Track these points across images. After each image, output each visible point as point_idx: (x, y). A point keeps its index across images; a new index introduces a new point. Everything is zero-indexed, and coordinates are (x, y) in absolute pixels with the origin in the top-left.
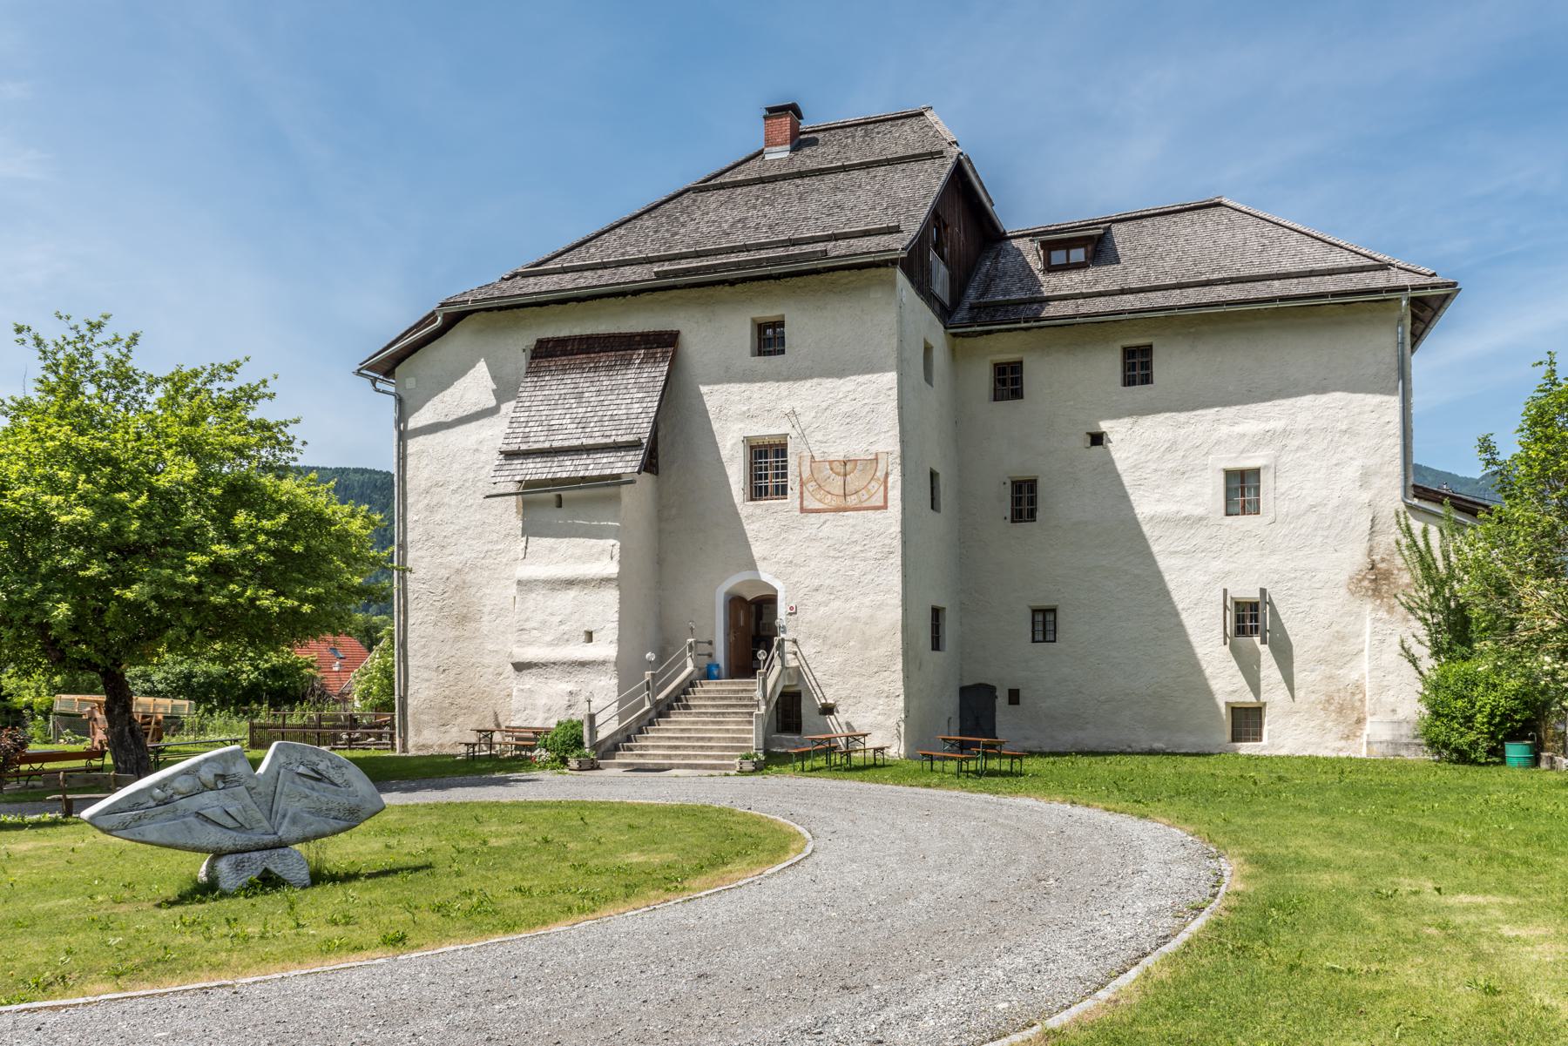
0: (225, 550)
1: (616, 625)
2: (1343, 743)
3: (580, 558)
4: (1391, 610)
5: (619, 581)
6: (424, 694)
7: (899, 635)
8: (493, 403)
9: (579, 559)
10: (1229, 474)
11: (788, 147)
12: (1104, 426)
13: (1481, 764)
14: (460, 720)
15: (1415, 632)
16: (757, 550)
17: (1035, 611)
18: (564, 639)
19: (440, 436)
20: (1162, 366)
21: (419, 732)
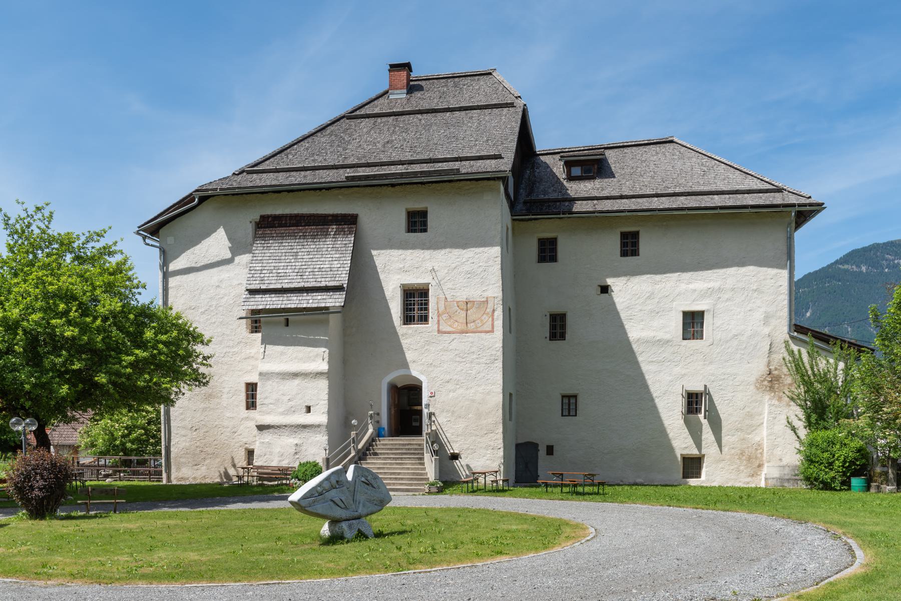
0: (141, 353)
2: (749, 479)
4: (780, 399)
5: (328, 375)
6: (183, 445)
7: (501, 411)
8: (229, 255)
10: (685, 314)
11: (405, 91)
12: (610, 281)
13: (836, 490)
14: (207, 461)
15: (796, 414)
16: (409, 356)
17: (563, 397)
18: (292, 411)
19: (191, 276)
20: (645, 244)
21: (178, 469)
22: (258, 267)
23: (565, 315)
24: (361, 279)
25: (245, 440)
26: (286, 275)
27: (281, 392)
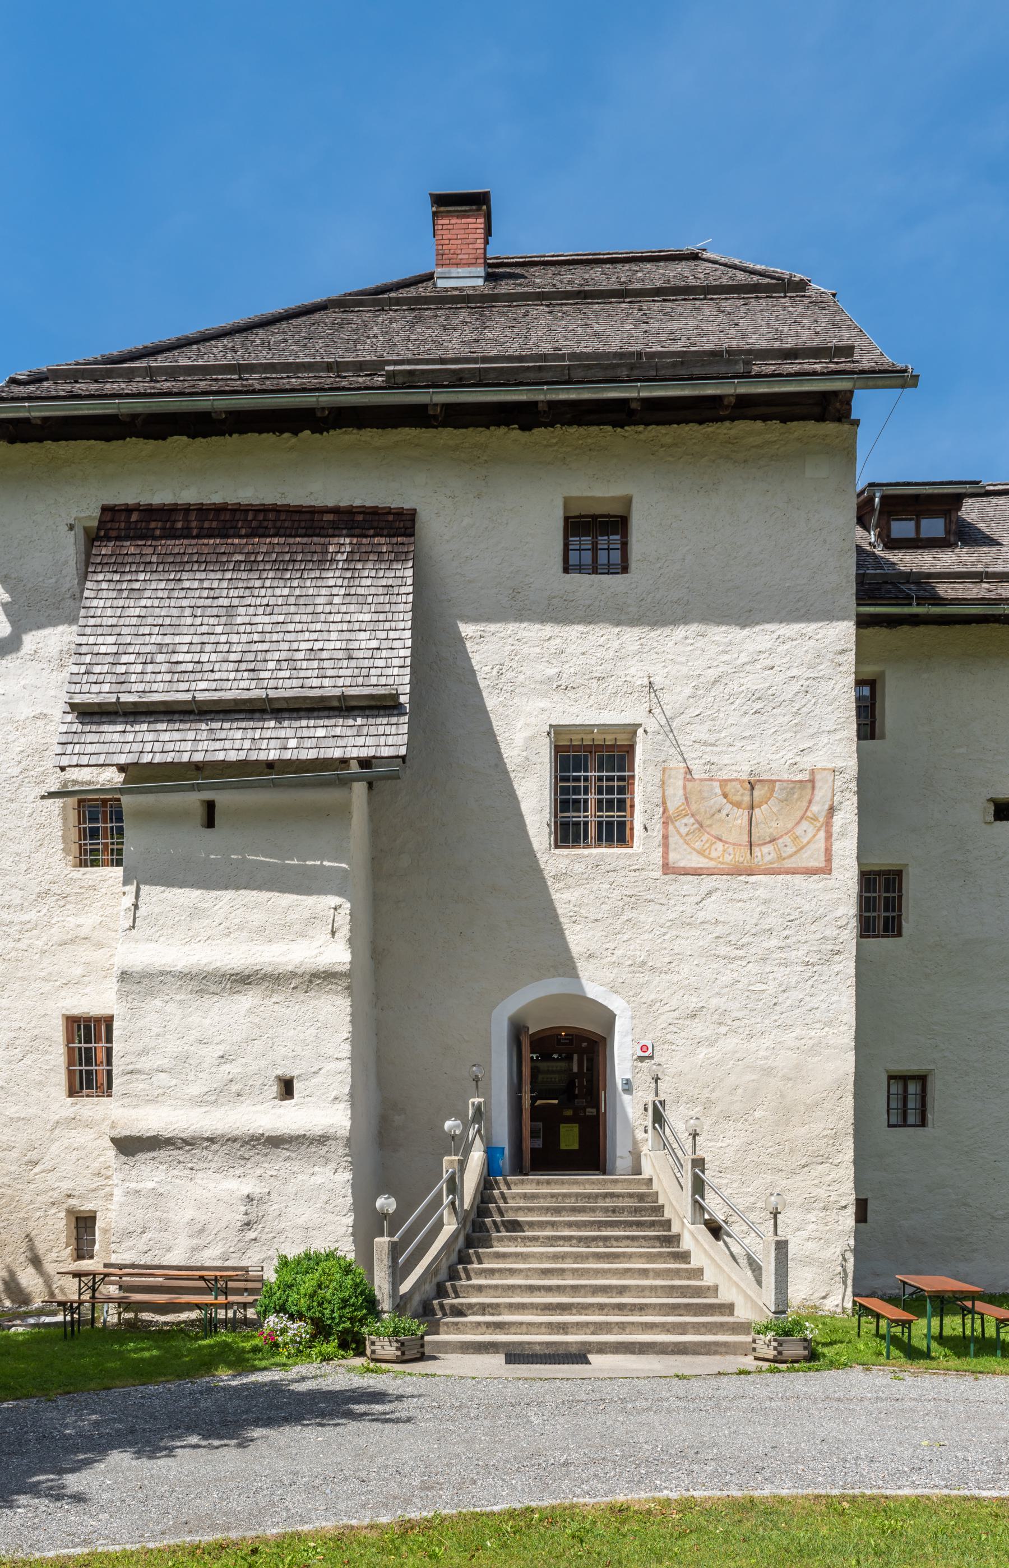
1: (345, 1065)
3: (261, 930)
7: (849, 1101)
9: (260, 933)
16: (578, 939)
22: (107, 644)
23: (899, 873)
24: (440, 691)
25: (66, 1185)
26: (199, 668)
27: (195, 1034)
